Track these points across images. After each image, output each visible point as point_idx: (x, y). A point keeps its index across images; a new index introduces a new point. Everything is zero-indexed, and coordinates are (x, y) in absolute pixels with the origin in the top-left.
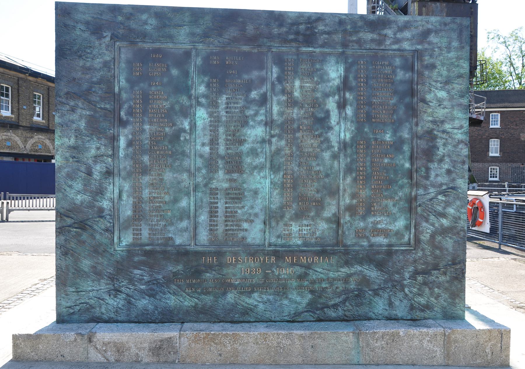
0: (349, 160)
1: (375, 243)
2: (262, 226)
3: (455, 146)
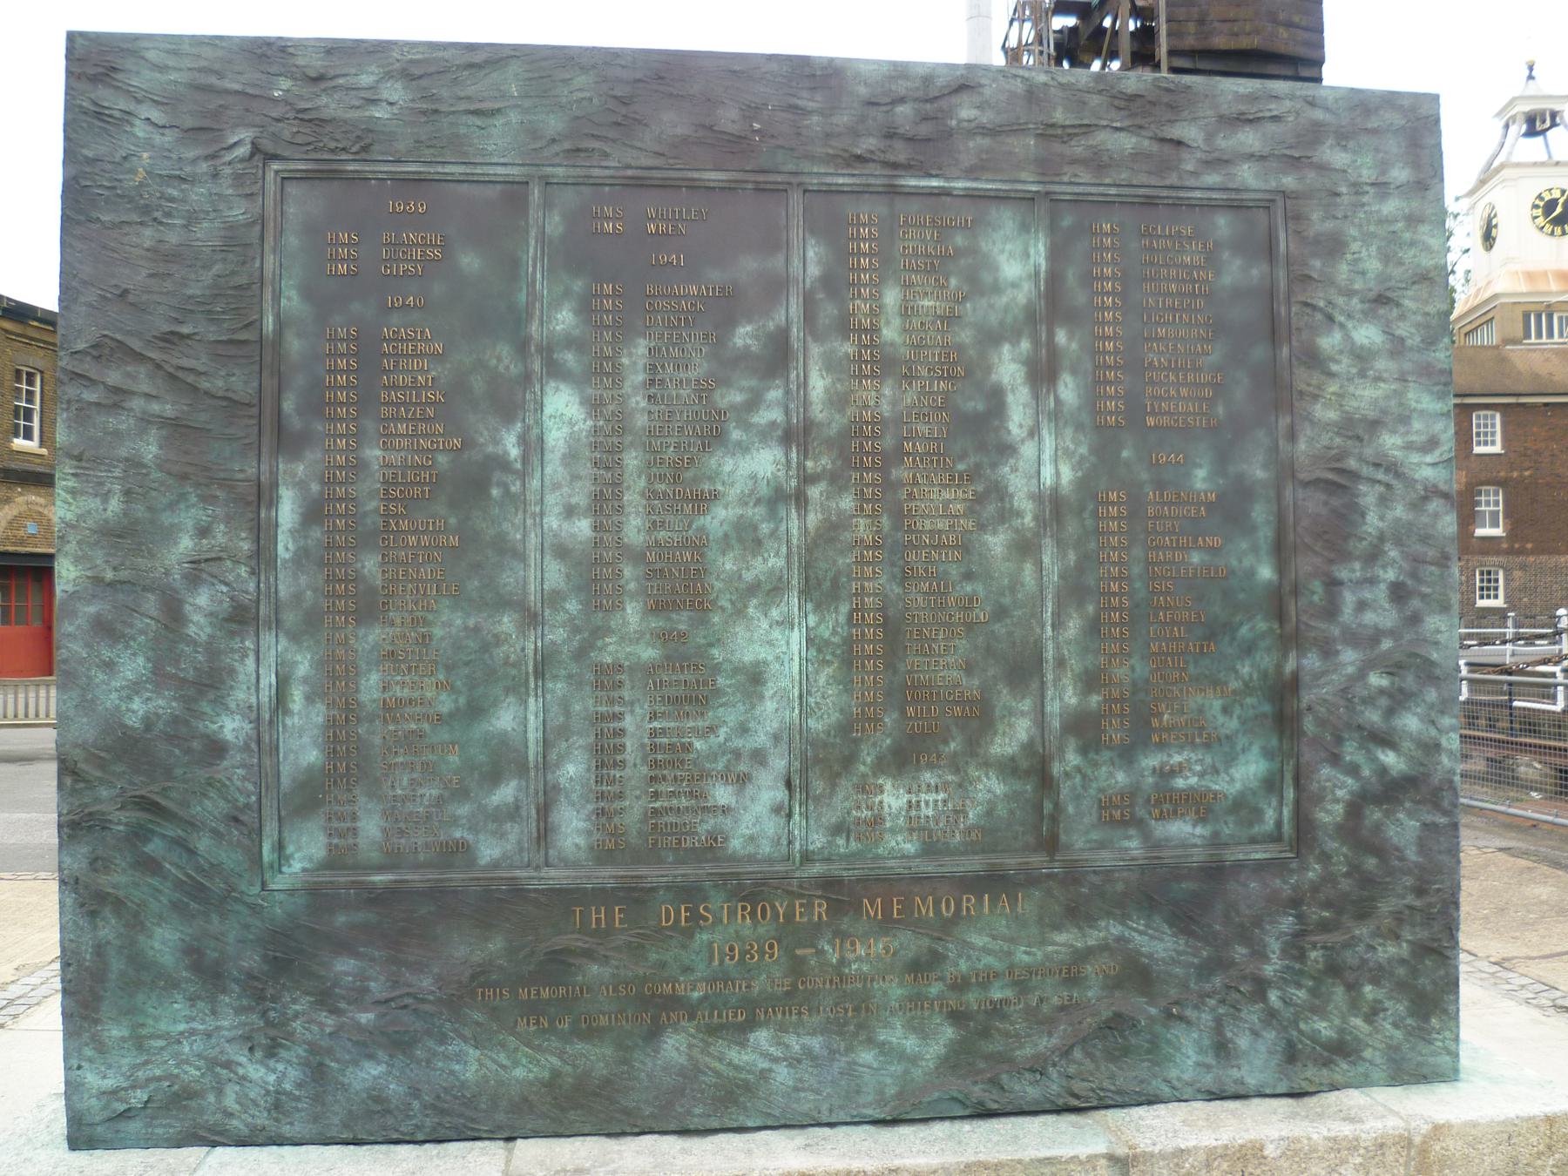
0: (1072, 557)
1: (1167, 839)
2: (781, 794)
3: (1417, 505)
